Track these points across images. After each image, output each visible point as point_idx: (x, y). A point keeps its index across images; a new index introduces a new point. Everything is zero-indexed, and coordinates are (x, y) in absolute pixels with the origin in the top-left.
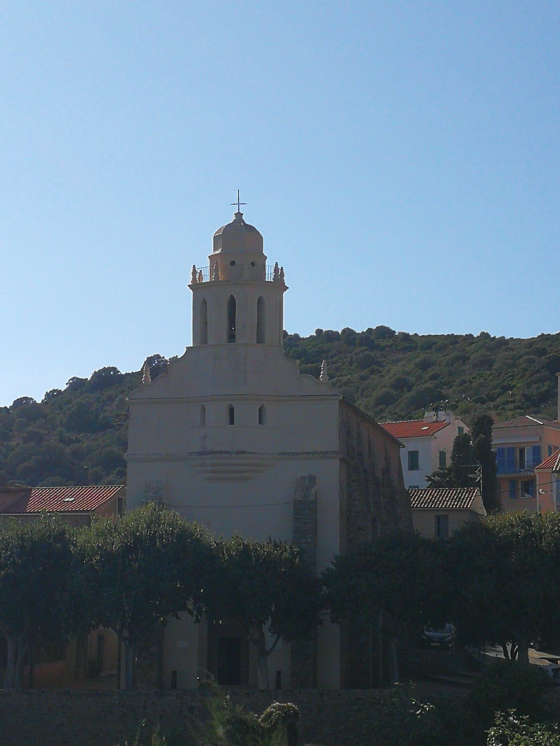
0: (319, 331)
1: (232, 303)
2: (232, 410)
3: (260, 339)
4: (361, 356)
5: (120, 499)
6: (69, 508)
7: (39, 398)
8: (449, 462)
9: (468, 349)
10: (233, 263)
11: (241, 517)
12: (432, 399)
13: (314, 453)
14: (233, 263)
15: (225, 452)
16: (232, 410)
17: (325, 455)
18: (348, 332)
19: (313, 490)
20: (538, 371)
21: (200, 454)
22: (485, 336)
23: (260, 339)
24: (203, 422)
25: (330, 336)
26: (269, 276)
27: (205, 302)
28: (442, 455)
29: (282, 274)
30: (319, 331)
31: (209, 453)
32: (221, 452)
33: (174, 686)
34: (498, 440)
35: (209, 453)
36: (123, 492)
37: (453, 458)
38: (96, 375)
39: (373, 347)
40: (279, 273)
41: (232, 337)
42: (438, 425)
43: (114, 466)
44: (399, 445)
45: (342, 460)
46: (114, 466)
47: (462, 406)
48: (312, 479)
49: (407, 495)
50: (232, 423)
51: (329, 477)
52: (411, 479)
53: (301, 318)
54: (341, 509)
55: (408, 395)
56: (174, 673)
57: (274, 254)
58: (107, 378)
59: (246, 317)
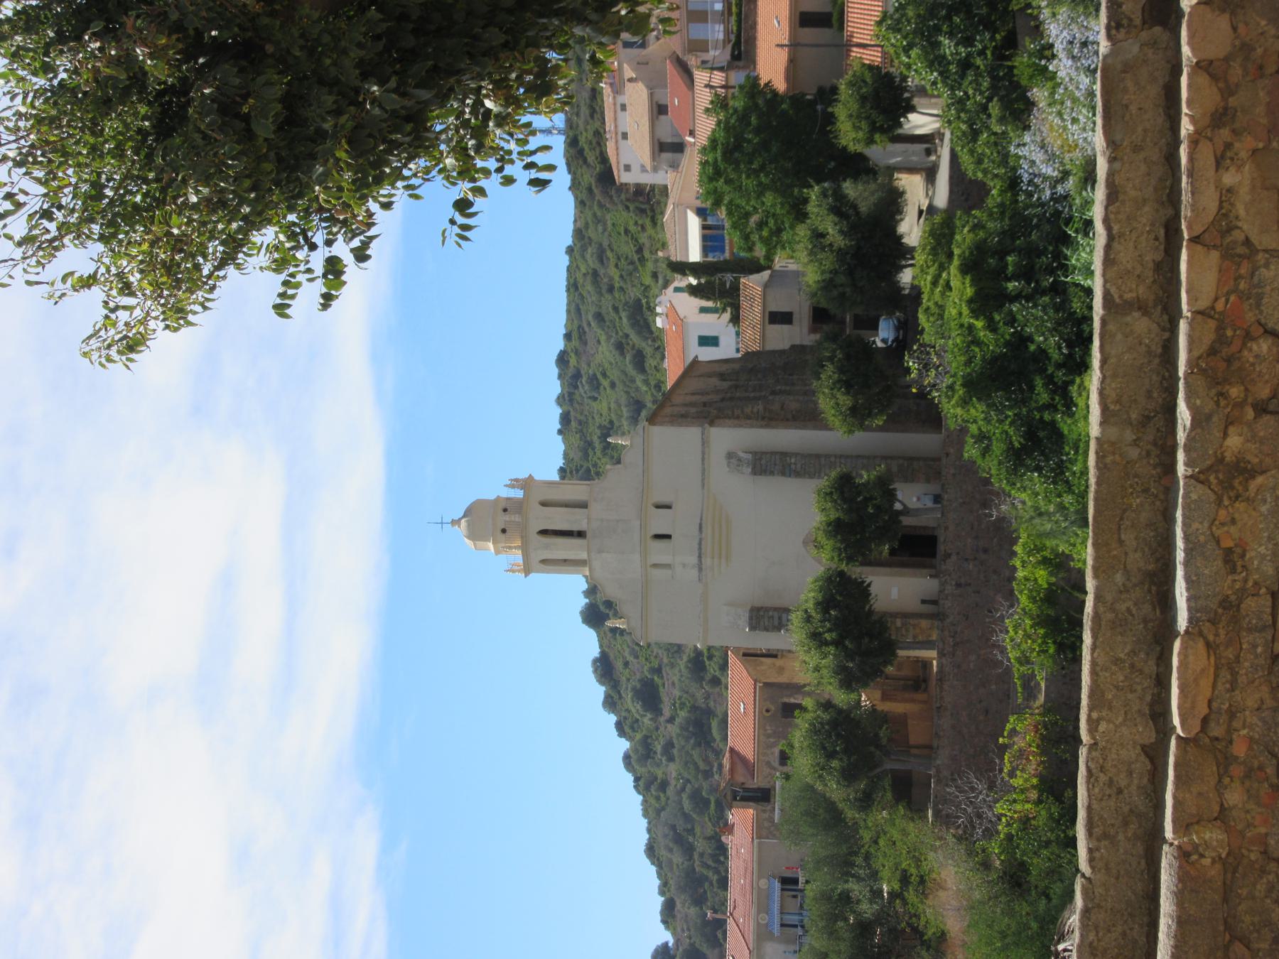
0: (560, 432)
1: (544, 532)
2: (658, 537)
3: (583, 505)
4: (586, 387)
5: (745, 655)
6: (751, 707)
7: (625, 745)
8: (710, 304)
9: (584, 271)
10: (504, 531)
11: (780, 536)
12: (641, 314)
13: (703, 453)
14: (504, 531)
15: (700, 544)
16: (658, 537)
17: (705, 443)
18: (560, 400)
19: (741, 455)
20: (611, 197)
21: (700, 570)
22: (570, 251)
23: (583, 505)
24: (668, 566)
25: (565, 419)
26: (518, 494)
27: (544, 561)
28: (703, 310)
29: (516, 480)
30: (560, 432)
31: (700, 561)
32: (700, 548)
33: (934, 602)
34: (695, 255)
35: (700, 561)
36: (736, 650)
37: (708, 299)
38: (601, 682)
39: (577, 376)
40: (515, 483)
41: (581, 534)
42: (672, 312)
43: (705, 667)
44: (695, 362)
45: (712, 424)
46: (705, 667)
47: (648, 280)
48: (730, 456)
49: (748, 356)
50: (668, 537)
51: (729, 438)
52: (727, 349)
53: (545, 456)
54: (761, 427)
55: (634, 338)
56: (923, 602)
57: (496, 488)
58: (605, 668)
59: (560, 519)
